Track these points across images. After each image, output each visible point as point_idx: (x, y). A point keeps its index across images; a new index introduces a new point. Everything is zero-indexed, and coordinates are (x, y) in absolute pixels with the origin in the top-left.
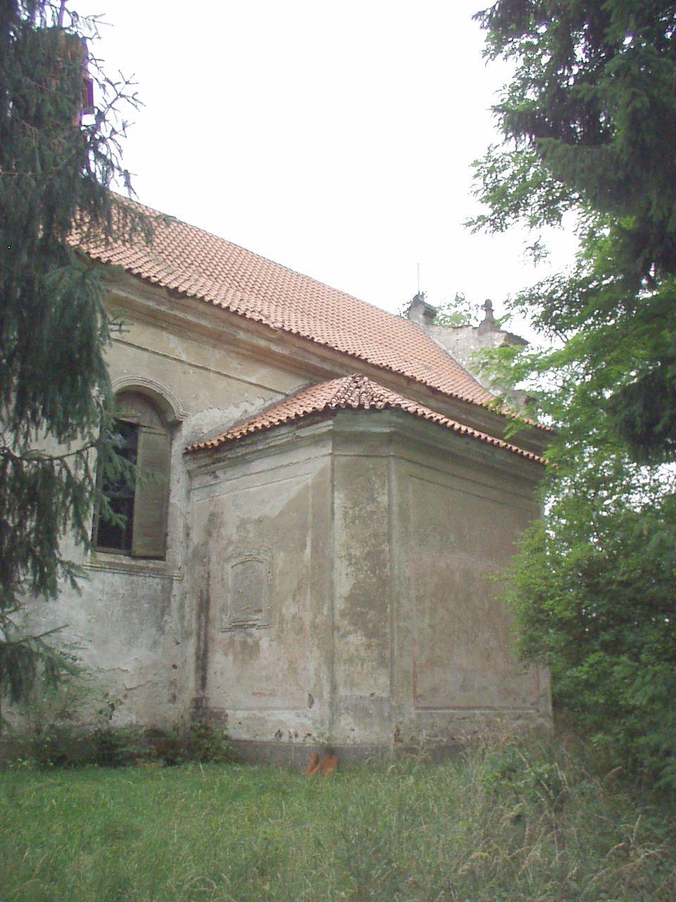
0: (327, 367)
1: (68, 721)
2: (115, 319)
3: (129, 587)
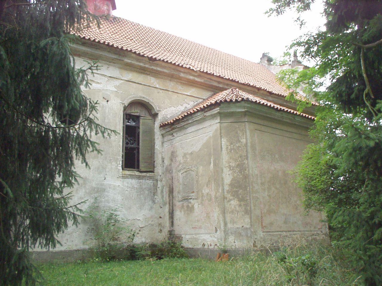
0: (221, 86)
1: (116, 242)
2: (94, 64)
3: (139, 185)
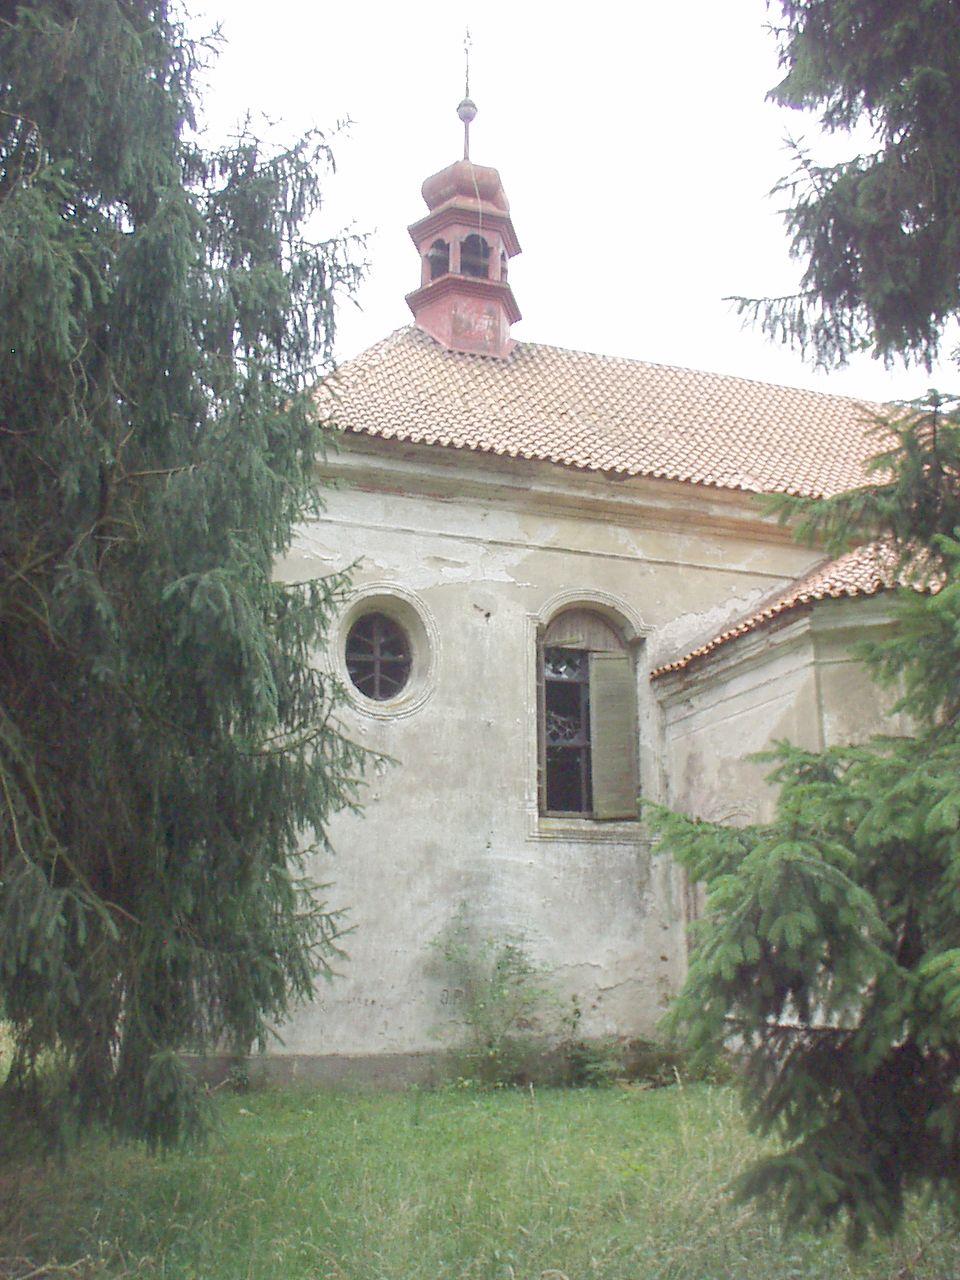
1: (527, 1032)
3: (593, 860)
